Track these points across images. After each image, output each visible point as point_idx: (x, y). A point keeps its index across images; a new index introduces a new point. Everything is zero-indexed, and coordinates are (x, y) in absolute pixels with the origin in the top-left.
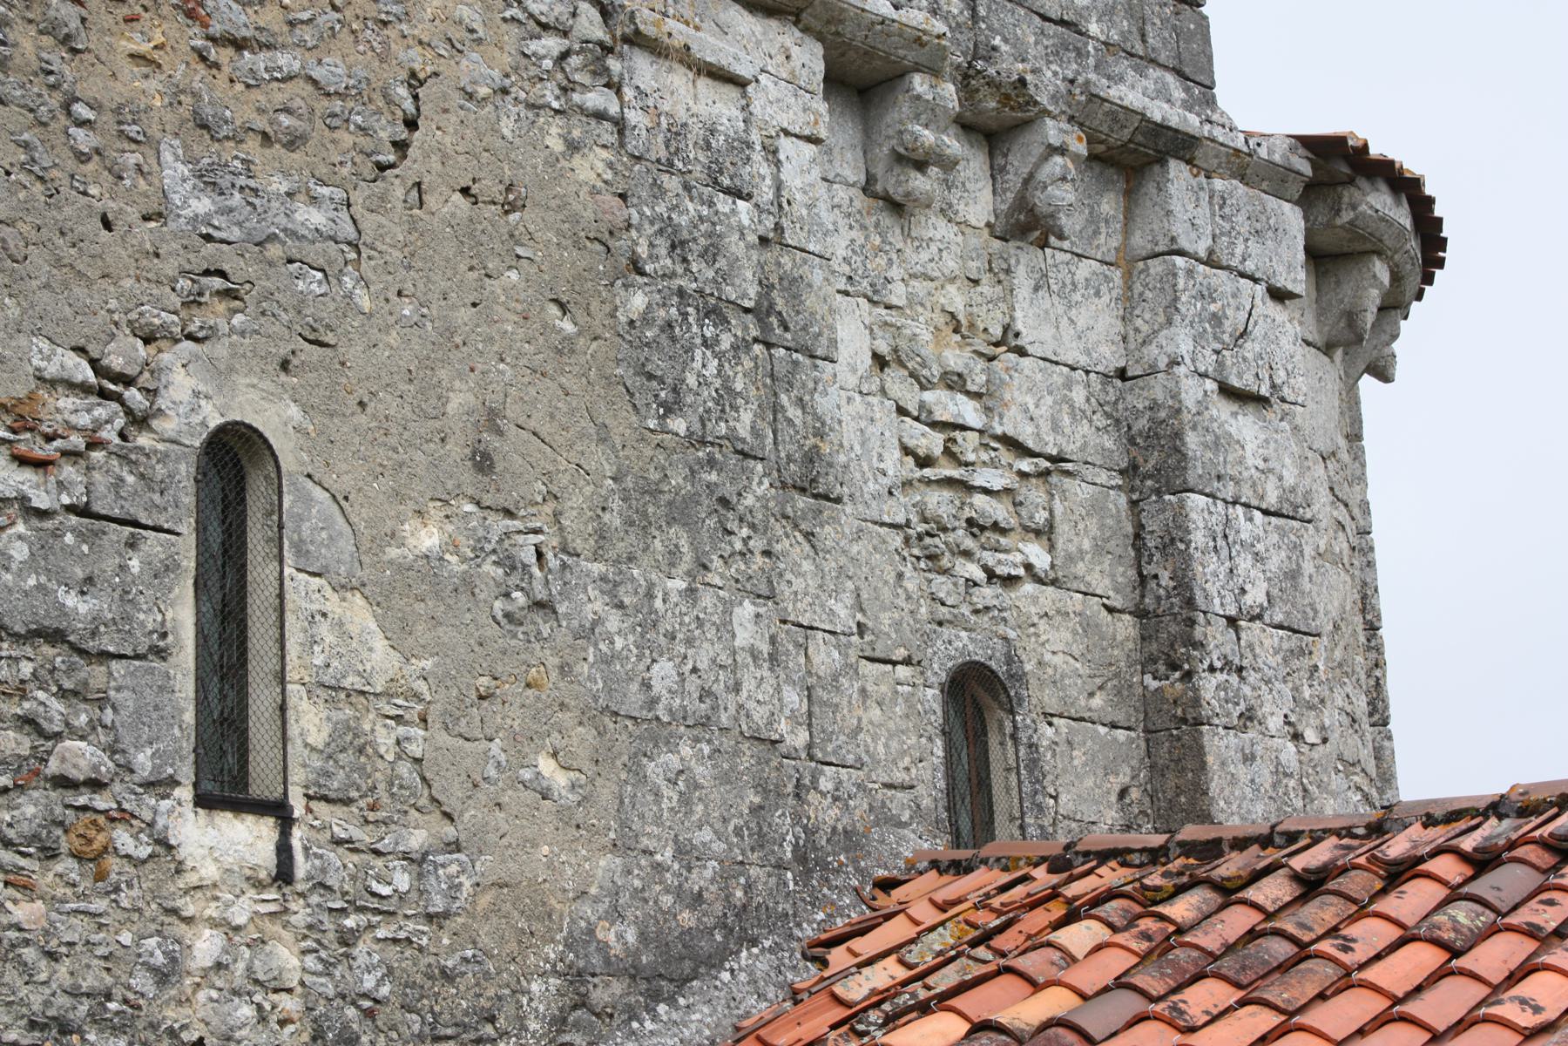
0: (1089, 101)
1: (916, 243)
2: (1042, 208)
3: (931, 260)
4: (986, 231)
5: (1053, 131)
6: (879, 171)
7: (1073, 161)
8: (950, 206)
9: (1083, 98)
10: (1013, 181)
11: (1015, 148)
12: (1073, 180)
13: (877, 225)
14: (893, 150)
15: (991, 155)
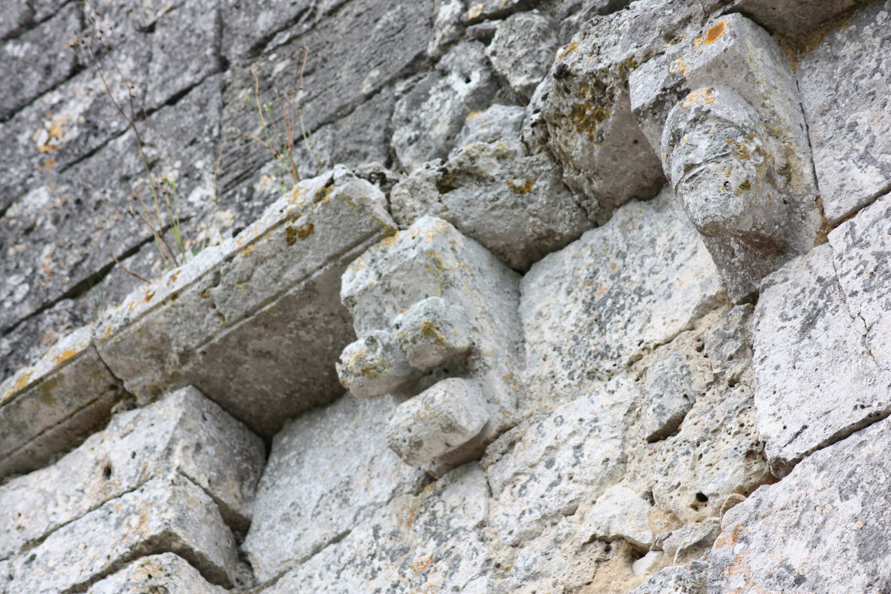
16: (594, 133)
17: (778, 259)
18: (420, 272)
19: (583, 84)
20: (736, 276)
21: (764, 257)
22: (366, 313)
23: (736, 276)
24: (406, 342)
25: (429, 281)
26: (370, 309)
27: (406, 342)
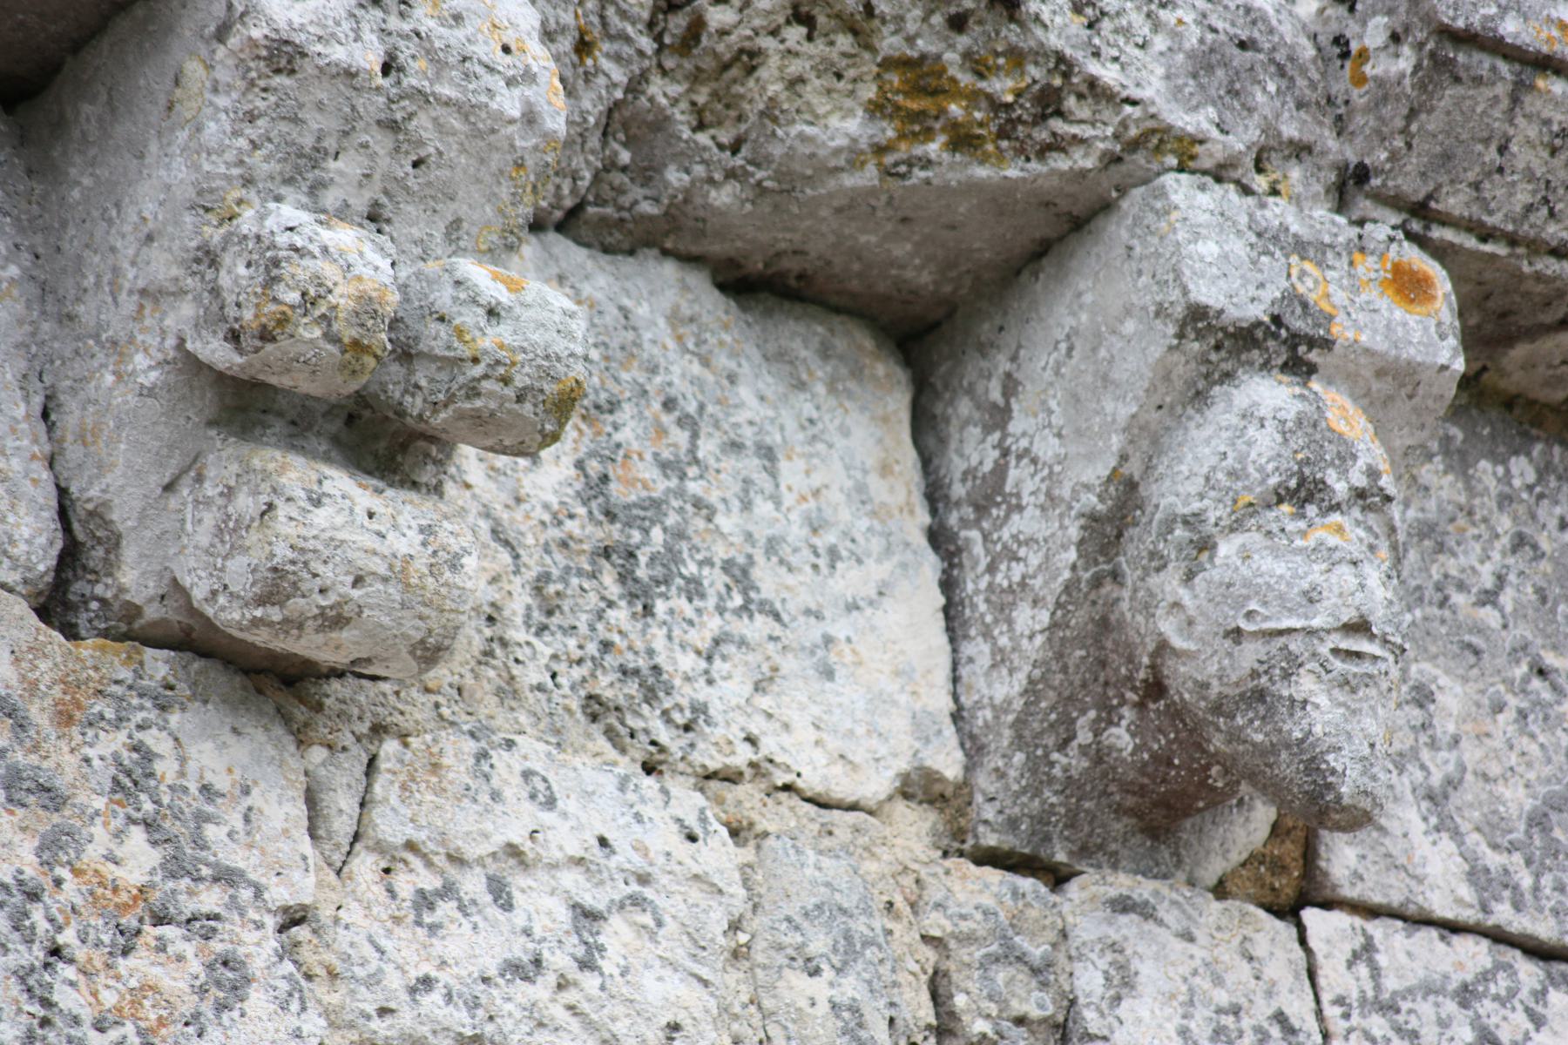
0: (1436, 70)
1: (415, 879)
2: (1205, 667)
3: (526, 969)
4: (913, 830)
5: (1206, 245)
6: (119, 483)
7: (1376, 407)
8: (653, 684)
9: (1405, 62)
10: (1040, 541)
11: (1039, 364)
12: (1367, 498)
13: (131, 779)
14: (191, 365)
15: (926, 426)
16: (903, 150)
17: (1136, 840)
18: (496, 160)
19: (1017, 58)
20: (1037, 793)
21: (1119, 811)
22: (295, 120)
23: (1037, 793)
24: (506, 381)
25: (492, 197)
26: (315, 121)
27: (506, 381)
